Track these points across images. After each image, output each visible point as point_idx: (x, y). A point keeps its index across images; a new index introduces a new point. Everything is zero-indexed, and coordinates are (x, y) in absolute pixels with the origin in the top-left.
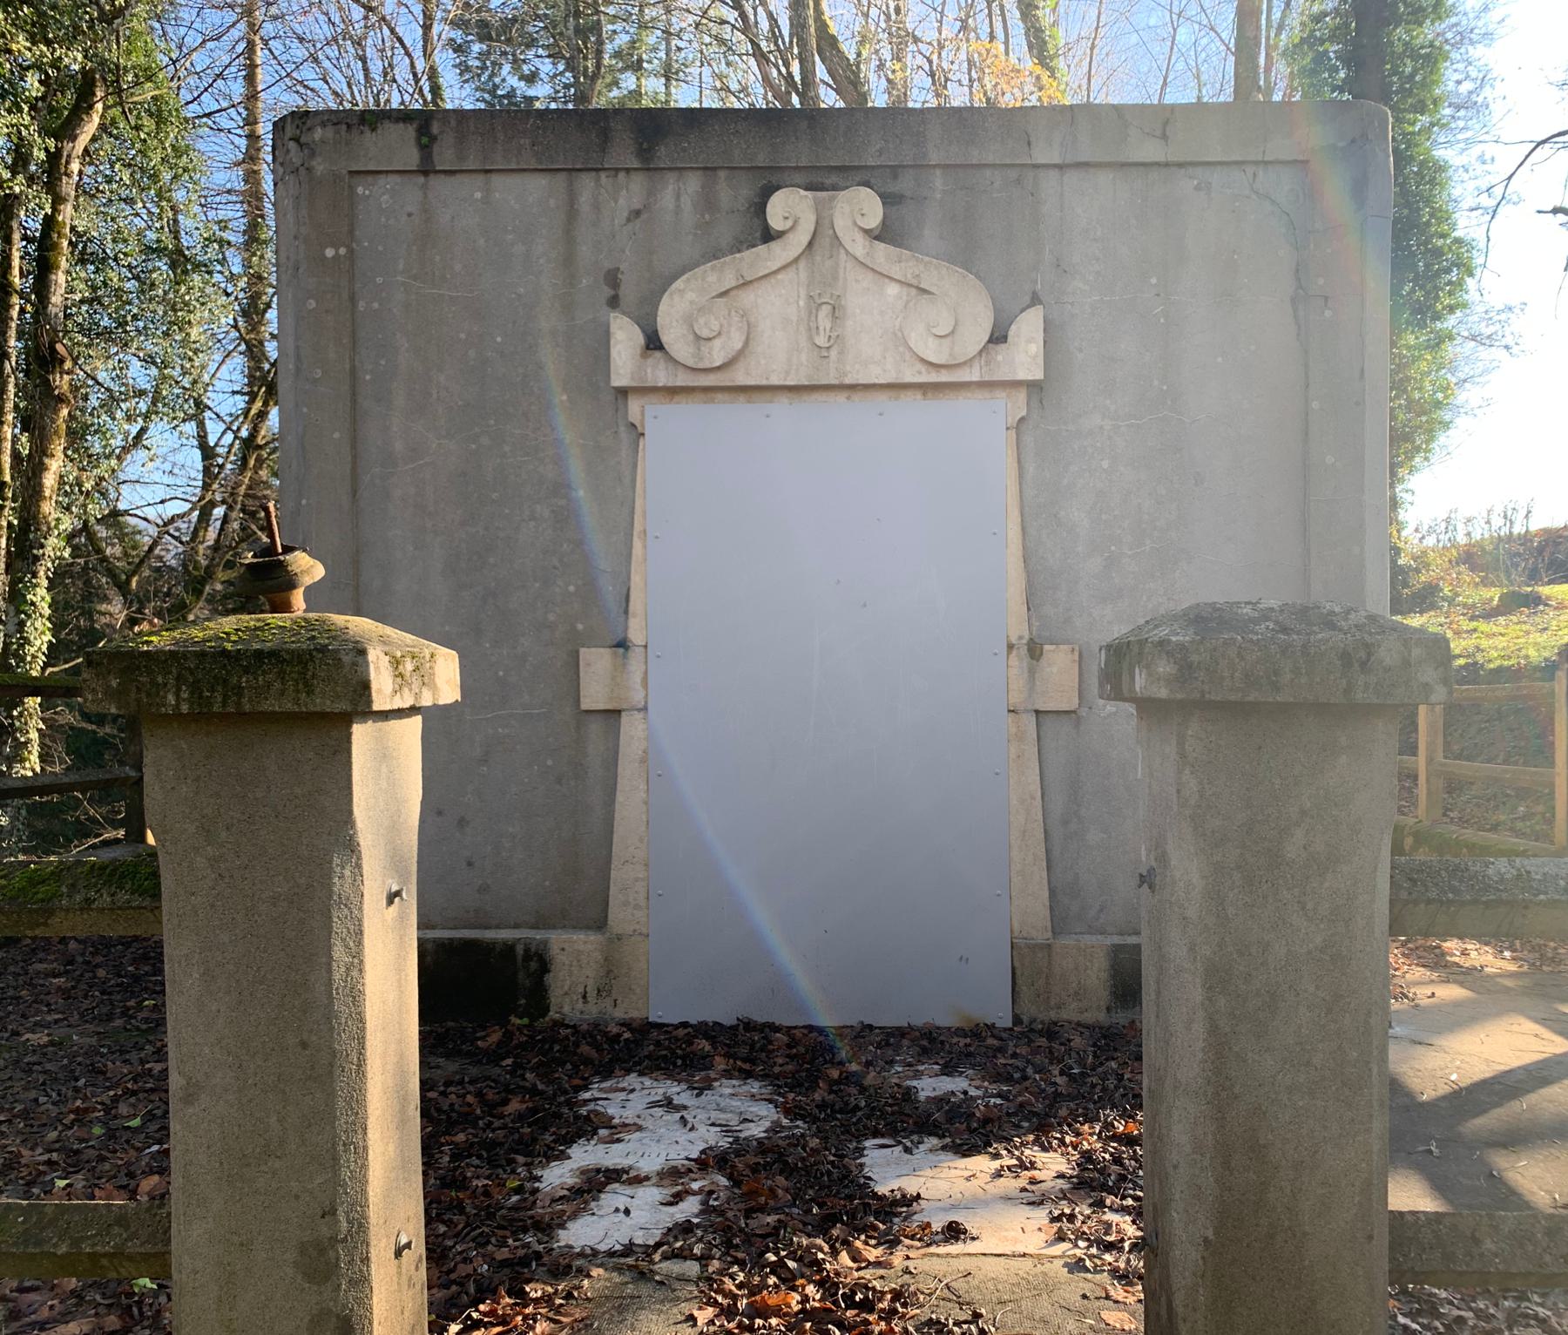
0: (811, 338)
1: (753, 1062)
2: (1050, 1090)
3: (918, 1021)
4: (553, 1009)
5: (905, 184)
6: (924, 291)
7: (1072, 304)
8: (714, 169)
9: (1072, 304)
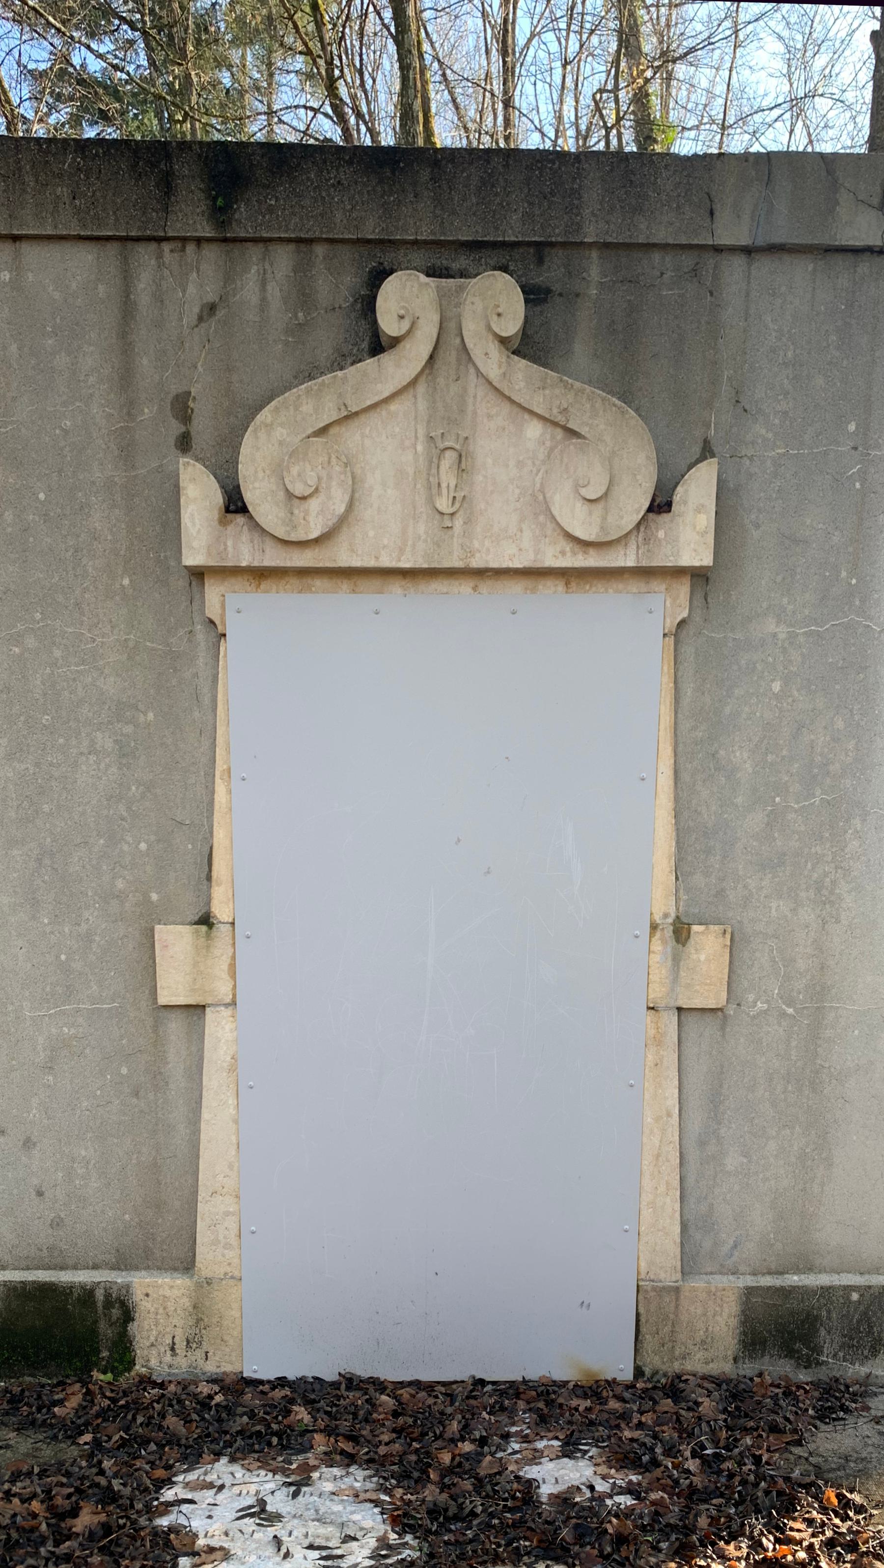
0: (430, 501)
1: (353, 1438)
2: (684, 1483)
3: (534, 1374)
4: (139, 1362)
5: (551, 274)
6: (572, 433)
7: (751, 458)
8: (310, 241)
9: (751, 458)
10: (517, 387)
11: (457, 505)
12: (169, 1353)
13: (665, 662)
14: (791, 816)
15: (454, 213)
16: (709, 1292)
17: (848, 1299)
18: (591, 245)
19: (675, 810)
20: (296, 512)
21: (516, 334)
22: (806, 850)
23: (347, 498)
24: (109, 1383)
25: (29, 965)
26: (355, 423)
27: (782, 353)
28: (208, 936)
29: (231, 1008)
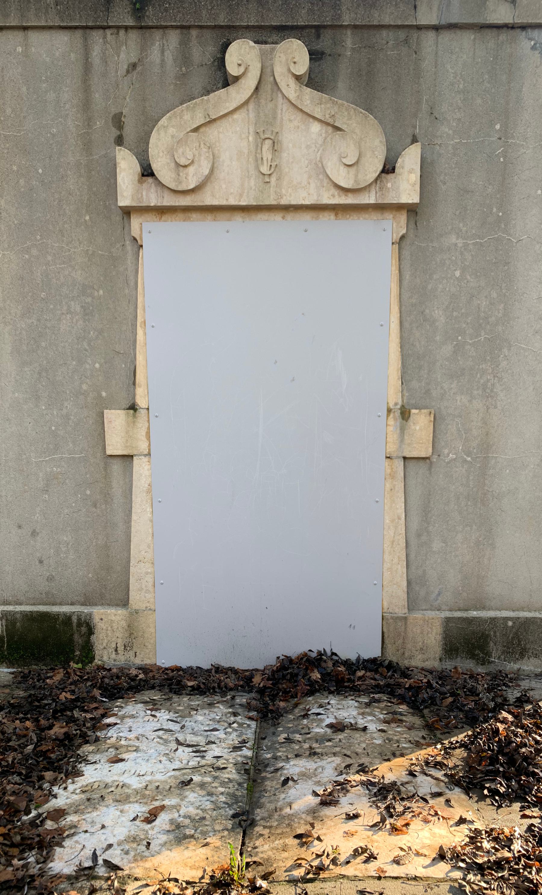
0: (257, 168)
4: (97, 657)
5: (325, 43)
7: (440, 145)
8: (188, 27)
9: (440, 145)
10: (305, 103)
11: (272, 170)
12: (114, 653)
13: (394, 258)
14: (468, 347)
15: (269, 10)
16: (424, 620)
17: (506, 625)
18: (347, 27)
19: (401, 343)
20: (181, 174)
21: (305, 73)
22: (477, 367)
23: (209, 166)
24: (79, 669)
25: (34, 433)
26: (214, 126)
27: (457, 86)
28: (134, 416)
29: (147, 457)
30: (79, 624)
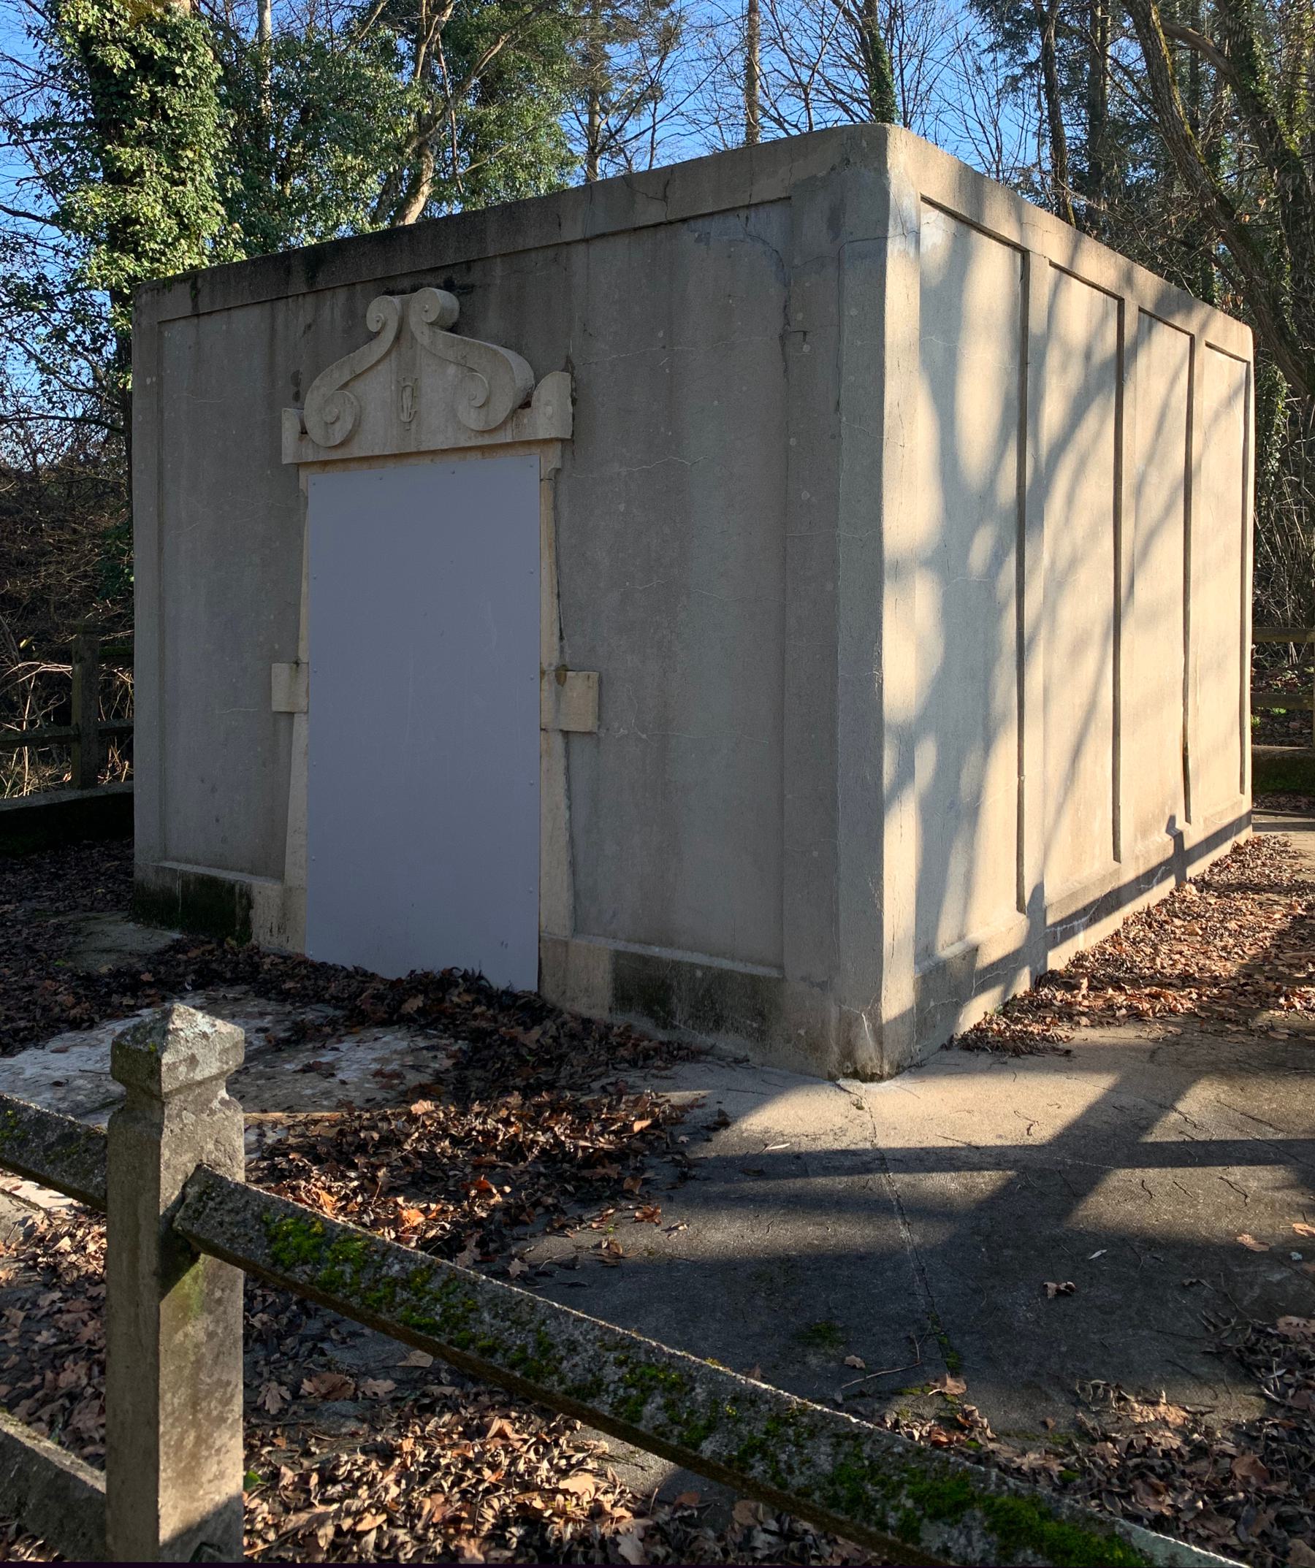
5: (475, 276)
18: (495, 257)
30: (241, 896)
